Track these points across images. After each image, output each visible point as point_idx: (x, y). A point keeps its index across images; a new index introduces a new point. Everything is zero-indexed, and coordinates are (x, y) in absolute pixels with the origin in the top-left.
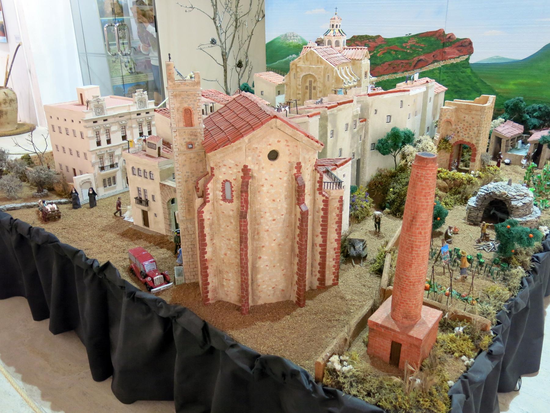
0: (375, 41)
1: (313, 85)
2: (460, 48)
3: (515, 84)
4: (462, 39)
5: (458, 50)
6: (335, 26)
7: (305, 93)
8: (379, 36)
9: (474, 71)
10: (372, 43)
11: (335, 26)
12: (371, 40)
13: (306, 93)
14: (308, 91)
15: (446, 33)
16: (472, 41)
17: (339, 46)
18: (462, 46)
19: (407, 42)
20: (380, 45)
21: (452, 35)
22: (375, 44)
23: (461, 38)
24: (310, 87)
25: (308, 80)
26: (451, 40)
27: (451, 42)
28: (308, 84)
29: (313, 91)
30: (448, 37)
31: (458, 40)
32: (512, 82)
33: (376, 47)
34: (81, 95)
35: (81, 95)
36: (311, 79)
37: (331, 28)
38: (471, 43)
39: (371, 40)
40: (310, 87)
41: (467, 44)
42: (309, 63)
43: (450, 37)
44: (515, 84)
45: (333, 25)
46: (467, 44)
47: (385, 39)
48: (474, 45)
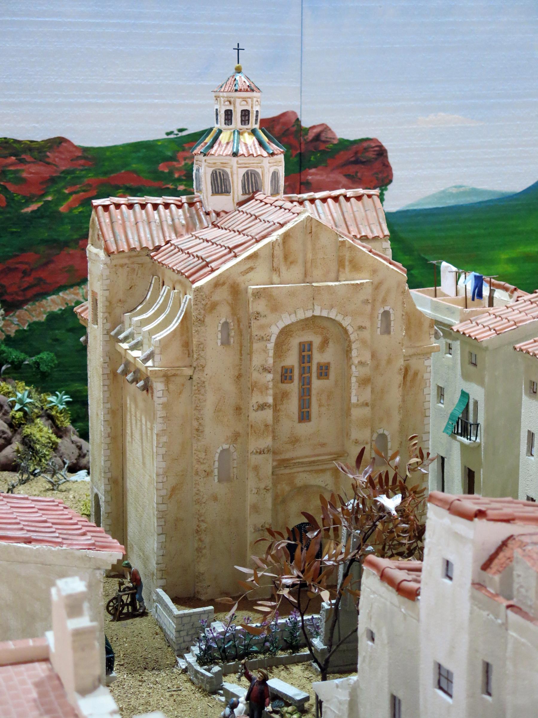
0: (42, 160)
1: (317, 358)
2: (352, 169)
3: (512, 261)
4: (355, 142)
5: (347, 176)
6: (237, 117)
7: (281, 397)
8: (61, 141)
9: (402, 235)
10: (34, 168)
11: (237, 117)
12: (26, 157)
13: (285, 395)
14: (294, 388)
15: (306, 123)
16: (385, 145)
17: (227, 192)
18: (357, 162)
19: (173, 158)
20: (67, 172)
21: (325, 128)
22: (43, 171)
23: (352, 138)
24: (305, 370)
25: (295, 342)
26: (322, 147)
27: (323, 152)
28: (292, 359)
29: (316, 384)
30: (311, 135)
31: (345, 144)
32: (504, 256)
33: (53, 180)
34: (487, 668)
35: (487, 668)
36: (307, 337)
37: (221, 125)
38: (382, 152)
39: (26, 157)
40: (305, 370)
41: (371, 155)
42: (296, 271)
43: (317, 137)
44: (512, 261)
45: (229, 114)
46: (371, 155)
47: (86, 150)
48: (392, 159)
